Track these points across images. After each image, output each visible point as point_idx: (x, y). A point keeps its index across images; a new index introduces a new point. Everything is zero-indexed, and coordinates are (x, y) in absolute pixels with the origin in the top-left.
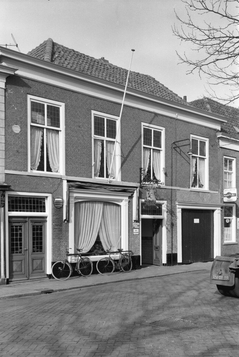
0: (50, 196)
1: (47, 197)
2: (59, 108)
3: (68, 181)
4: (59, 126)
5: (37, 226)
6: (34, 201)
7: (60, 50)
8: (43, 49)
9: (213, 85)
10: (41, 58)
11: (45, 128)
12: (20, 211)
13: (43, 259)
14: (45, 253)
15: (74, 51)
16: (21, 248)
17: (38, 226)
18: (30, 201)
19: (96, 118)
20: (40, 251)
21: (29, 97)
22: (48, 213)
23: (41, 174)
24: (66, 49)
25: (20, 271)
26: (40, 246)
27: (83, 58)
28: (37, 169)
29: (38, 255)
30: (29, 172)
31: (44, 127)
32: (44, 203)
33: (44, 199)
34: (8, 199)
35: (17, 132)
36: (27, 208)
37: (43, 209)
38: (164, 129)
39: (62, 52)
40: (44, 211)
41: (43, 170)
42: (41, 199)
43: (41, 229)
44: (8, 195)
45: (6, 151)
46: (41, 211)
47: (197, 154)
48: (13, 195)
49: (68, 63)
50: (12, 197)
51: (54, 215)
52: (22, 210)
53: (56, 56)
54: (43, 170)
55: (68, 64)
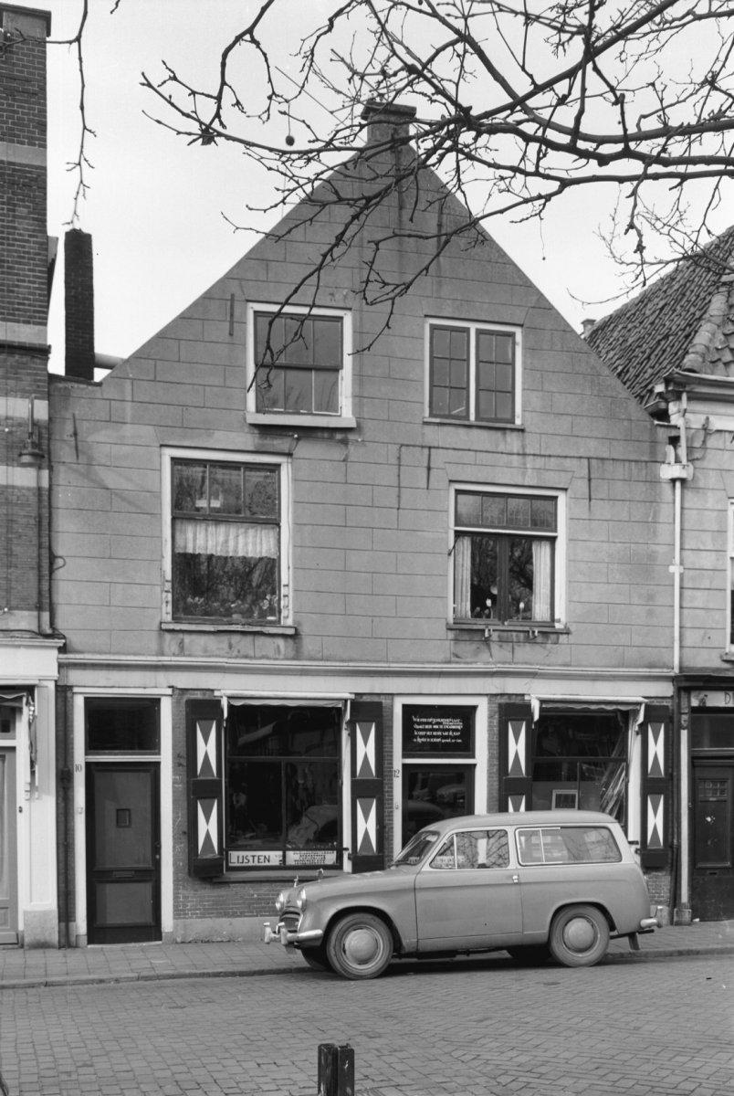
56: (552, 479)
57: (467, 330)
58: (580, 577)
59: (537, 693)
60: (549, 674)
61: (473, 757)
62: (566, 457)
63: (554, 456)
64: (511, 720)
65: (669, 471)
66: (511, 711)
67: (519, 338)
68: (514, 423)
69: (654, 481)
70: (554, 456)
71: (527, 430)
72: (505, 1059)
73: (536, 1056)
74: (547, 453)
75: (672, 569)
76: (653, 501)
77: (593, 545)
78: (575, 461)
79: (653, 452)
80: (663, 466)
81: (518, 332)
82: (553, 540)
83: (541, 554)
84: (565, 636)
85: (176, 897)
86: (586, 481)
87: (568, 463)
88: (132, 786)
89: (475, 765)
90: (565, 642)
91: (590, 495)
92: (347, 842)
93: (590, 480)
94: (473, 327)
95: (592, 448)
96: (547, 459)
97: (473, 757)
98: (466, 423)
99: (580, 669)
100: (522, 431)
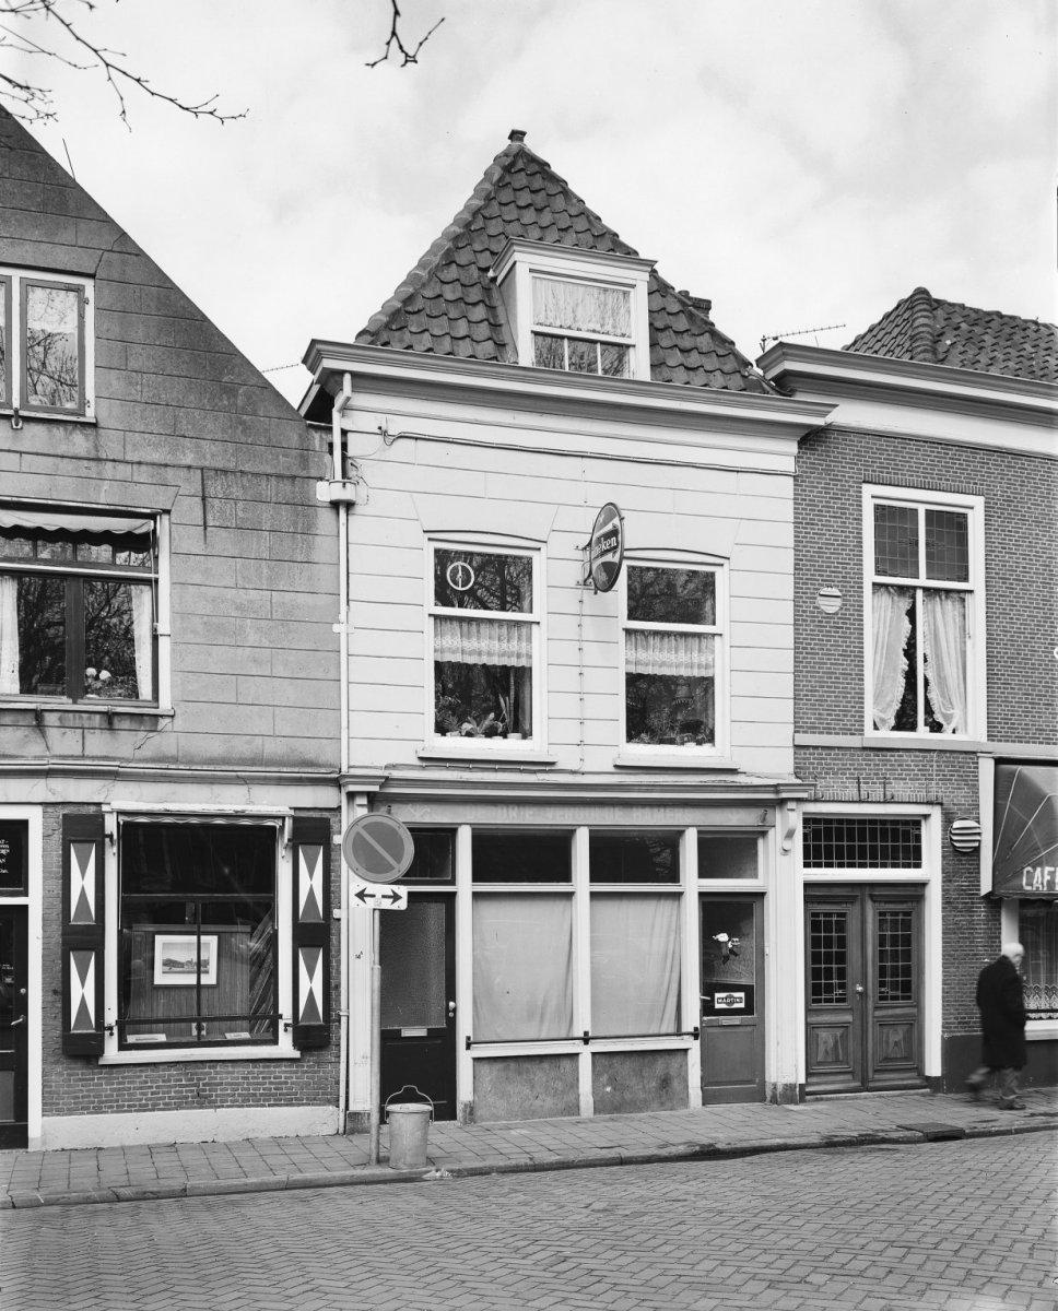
0: (936, 814)
1: (926, 817)
2: (964, 516)
3: (999, 761)
4: (967, 575)
5: (826, 915)
6: (839, 833)
7: (957, 319)
8: (900, 329)
9: (73, 37)
10: (876, 352)
11: (920, 587)
12: (841, 865)
13: (914, 1025)
14: (919, 1006)
15: (999, 314)
16: (842, 986)
17: (830, 915)
18: (862, 832)
19: (882, 512)
20: (903, 998)
21: (868, 490)
22: (930, 869)
23: (906, 739)
24: (973, 315)
25: (906, 1059)
26: (898, 976)
27: (1034, 336)
28: (892, 722)
29: (900, 1010)
30: (871, 736)
31: (917, 584)
32: (918, 839)
33: (915, 823)
34: (804, 828)
35: (832, 610)
36: (874, 857)
37: (913, 857)
38: (978, 502)
39: (964, 326)
40: (918, 866)
41: (913, 728)
42: (906, 823)
43: (907, 925)
44: (804, 813)
45: (796, 672)
46: (908, 866)
47: (916, 576)
48: (827, 814)
49: (991, 359)
50: (816, 821)
51: (947, 878)
52: (879, 861)
53: (948, 342)
54: (913, 728)
55: (991, 364)
56: (146, 499)
57: (10, 278)
58: (190, 637)
59: (124, 800)
60: (138, 775)
61: (26, 894)
62: (166, 465)
63: (147, 464)
64: (74, 842)
65: (325, 492)
66: (80, 828)
67: (90, 292)
68: (84, 415)
69: (307, 505)
70: (147, 464)
71: (102, 425)
72: (638, 1283)
73: (615, 1284)
74: (136, 459)
75: (336, 628)
76: (308, 531)
77: (212, 592)
78: (183, 473)
79: (304, 461)
80: (320, 484)
81: (89, 284)
82: (153, 583)
83: (141, 600)
84: (168, 720)
85: (44, 1074)
86: (198, 500)
87: (170, 472)
88: (436, 912)
89: (760, 896)
90: (169, 728)
91: (205, 523)
92: (285, 1007)
93: (204, 499)
94: (16, 274)
95: (214, 455)
96: (135, 467)
97: (26, 894)
98: (82, 419)
99: (212, 768)
100: (94, 425)
